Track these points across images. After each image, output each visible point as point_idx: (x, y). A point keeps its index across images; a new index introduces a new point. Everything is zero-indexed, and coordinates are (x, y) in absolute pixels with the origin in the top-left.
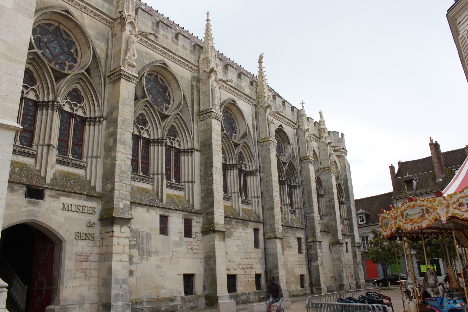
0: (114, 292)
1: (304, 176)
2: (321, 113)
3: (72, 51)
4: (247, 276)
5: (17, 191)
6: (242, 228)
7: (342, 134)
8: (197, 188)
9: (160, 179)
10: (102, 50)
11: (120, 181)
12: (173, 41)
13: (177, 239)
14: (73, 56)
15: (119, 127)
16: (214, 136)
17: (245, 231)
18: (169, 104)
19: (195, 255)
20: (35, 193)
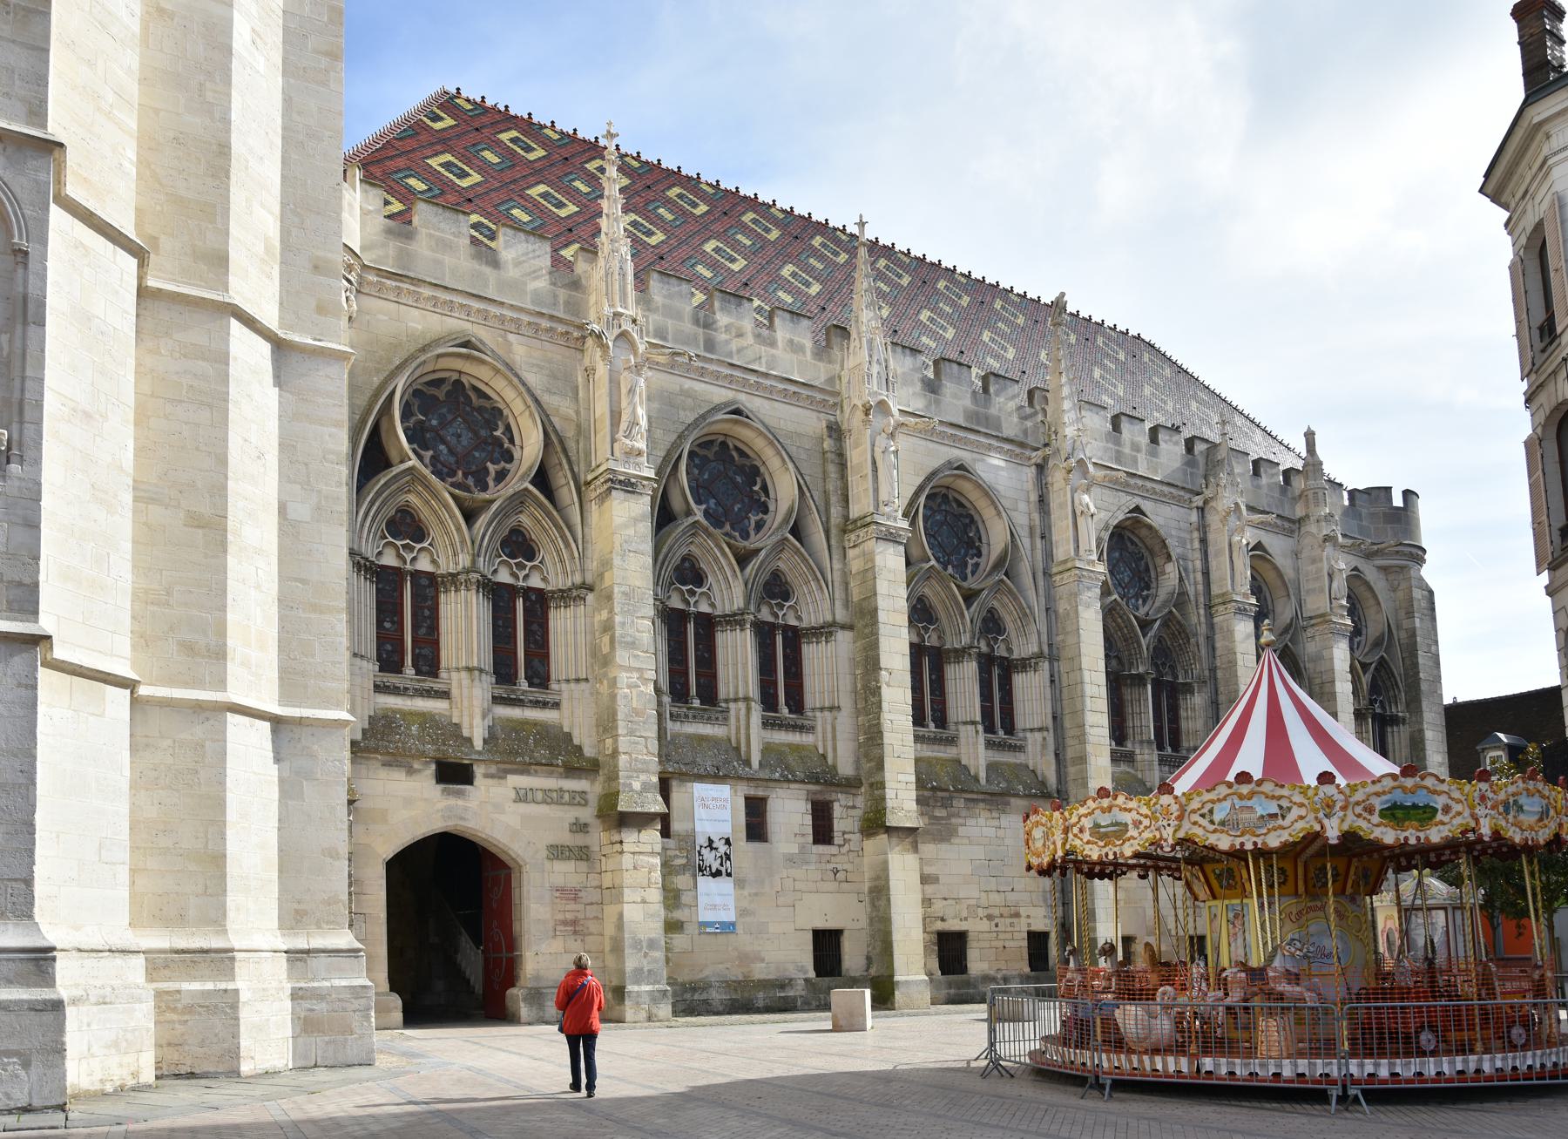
0: (630, 965)
1: (1218, 653)
2: (1310, 437)
3: (498, 433)
4: (1001, 936)
5: (419, 771)
6: (987, 814)
7: (1407, 494)
8: (845, 722)
9: (743, 712)
10: (566, 419)
11: (631, 733)
12: (758, 336)
13: (794, 849)
14: (501, 445)
15: (617, 609)
16: (882, 587)
17: (996, 823)
18: (766, 511)
19: (845, 885)
20: (454, 774)
